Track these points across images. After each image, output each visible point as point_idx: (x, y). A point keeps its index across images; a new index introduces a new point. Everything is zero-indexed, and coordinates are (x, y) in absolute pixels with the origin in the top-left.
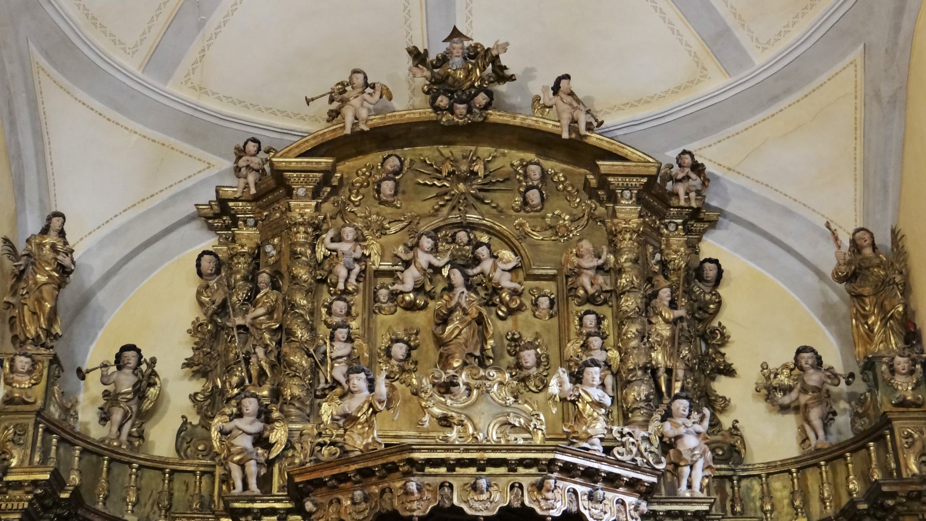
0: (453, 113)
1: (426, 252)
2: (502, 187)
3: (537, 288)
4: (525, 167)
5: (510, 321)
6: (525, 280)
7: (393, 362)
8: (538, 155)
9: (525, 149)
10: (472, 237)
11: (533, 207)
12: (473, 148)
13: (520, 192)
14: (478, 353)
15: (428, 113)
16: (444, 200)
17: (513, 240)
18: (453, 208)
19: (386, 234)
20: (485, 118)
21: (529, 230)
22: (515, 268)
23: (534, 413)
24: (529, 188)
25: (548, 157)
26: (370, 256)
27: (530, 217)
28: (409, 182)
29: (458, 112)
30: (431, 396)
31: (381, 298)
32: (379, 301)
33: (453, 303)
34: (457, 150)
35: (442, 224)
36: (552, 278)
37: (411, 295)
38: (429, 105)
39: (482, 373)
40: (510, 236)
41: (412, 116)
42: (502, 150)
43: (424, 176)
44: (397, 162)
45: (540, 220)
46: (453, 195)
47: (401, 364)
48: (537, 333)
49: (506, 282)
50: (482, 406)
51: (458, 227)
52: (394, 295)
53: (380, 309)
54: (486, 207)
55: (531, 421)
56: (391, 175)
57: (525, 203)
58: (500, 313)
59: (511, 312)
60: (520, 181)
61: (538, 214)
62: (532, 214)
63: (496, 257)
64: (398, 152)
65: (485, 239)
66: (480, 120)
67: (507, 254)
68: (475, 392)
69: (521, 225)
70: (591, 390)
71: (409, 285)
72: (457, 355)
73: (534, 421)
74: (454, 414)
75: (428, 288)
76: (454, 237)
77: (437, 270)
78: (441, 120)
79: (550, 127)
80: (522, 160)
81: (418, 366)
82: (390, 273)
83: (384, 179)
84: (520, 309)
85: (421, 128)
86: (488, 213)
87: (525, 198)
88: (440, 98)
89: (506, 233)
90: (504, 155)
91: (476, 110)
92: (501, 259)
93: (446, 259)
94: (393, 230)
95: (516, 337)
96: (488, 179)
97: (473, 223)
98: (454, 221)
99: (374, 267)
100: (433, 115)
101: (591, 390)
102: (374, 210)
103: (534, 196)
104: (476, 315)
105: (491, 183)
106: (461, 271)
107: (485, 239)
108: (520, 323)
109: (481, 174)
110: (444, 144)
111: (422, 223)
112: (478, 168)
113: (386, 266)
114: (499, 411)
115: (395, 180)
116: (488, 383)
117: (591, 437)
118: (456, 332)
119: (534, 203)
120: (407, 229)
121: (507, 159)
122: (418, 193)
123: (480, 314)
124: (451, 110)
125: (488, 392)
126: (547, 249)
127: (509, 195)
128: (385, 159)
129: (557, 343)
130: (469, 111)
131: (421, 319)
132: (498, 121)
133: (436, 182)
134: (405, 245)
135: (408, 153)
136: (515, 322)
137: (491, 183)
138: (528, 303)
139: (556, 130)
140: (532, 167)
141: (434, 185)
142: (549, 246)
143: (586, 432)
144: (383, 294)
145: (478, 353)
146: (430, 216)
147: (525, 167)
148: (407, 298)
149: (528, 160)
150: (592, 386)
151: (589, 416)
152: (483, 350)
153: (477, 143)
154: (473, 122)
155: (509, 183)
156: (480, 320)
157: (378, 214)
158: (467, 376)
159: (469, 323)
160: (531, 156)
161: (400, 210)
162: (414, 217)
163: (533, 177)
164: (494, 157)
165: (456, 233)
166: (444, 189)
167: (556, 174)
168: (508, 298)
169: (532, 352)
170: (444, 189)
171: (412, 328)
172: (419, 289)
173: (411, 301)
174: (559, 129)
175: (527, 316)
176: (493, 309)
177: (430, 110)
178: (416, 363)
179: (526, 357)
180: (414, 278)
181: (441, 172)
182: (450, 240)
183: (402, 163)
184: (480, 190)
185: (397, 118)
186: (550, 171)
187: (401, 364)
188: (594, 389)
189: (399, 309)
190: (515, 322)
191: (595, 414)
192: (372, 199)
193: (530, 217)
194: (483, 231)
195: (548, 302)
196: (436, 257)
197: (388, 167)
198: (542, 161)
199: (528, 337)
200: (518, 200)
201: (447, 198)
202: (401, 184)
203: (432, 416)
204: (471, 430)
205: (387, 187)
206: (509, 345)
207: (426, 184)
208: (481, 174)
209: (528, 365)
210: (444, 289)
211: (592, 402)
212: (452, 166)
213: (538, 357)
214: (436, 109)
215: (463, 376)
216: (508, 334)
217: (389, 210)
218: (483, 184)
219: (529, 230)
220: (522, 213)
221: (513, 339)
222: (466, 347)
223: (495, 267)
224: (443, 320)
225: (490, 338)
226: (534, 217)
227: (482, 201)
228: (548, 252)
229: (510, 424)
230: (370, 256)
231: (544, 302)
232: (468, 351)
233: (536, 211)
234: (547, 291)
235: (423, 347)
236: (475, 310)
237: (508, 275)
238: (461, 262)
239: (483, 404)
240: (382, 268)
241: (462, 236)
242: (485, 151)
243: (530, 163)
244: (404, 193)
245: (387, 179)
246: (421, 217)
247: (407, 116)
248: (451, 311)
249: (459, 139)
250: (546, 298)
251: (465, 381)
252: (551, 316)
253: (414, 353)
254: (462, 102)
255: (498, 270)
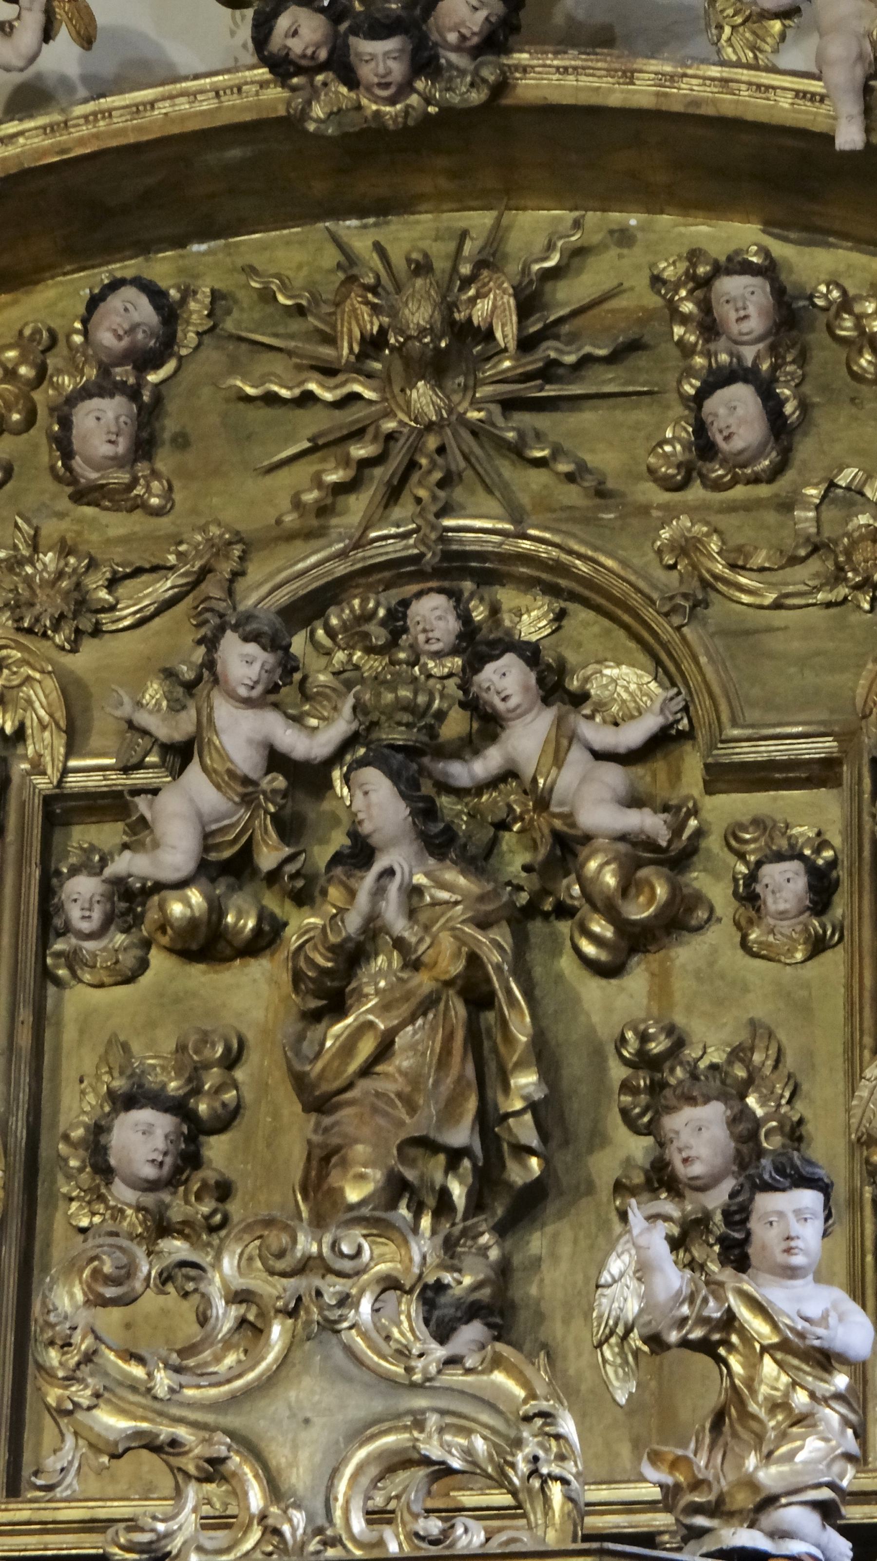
0: (351, 80)
1: (248, 703)
2: (608, 381)
3: (758, 823)
4: (702, 285)
5: (637, 981)
6: (710, 788)
7: (122, 1193)
8: (770, 225)
9: (712, 206)
10: (479, 614)
11: (738, 462)
12: (480, 221)
13: (684, 398)
14: (461, 1135)
15: (260, 93)
16: (346, 461)
17: (649, 614)
18: (394, 493)
19: (97, 631)
20: (501, 87)
21: (719, 568)
22: (662, 742)
23: (531, 1407)
24: (718, 379)
25: (816, 233)
26: (20, 734)
27: (732, 508)
28: (206, 391)
29: (366, 72)
30: (88, 1358)
31: (75, 913)
32: (67, 930)
33: (353, 923)
34: (410, 234)
35: (341, 569)
36: (821, 774)
37: (195, 896)
38: (250, 58)
39: (306, 1244)
40: (636, 600)
41: (183, 105)
42: (615, 217)
43: (278, 365)
44: (144, 311)
45: (771, 517)
46: (391, 437)
47: (149, 1199)
48: (753, 1025)
49: (597, 804)
50: (306, 1391)
51: (413, 577)
52: (129, 901)
53: (72, 959)
54: (538, 478)
55: (518, 1443)
56: (123, 373)
57: (704, 445)
58: (589, 949)
59: (638, 939)
60: (686, 350)
61: (763, 491)
62: (740, 492)
63: (580, 699)
64: (162, 267)
65: (532, 622)
66: (477, 97)
67: (625, 682)
68: (277, 1331)
69: (686, 548)
70: (779, 1295)
71: (175, 849)
72: (360, 1150)
73: (531, 1447)
74: (182, 1432)
75: (269, 855)
76: (397, 621)
77: (308, 778)
78: (304, 114)
79: (785, 102)
80: (694, 255)
81: (234, 1207)
82: (112, 805)
83: (85, 393)
84: (679, 919)
85: (235, 153)
86: (544, 504)
87: (701, 428)
88: (283, 22)
89: (619, 589)
90: (624, 238)
91: (453, 57)
92: (600, 707)
93: (341, 727)
94: (127, 614)
95: (656, 1047)
96: (549, 350)
97: (481, 556)
98: (393, 550)
99: (42, 783)
100: (275, 93)
101: (779, 1295)
102: (51, 529)
103: (738, 414)
104: (457, 968)
105: (549, 371)
106: (394, 776)
107: (532, 622)
108: (682, 986)
109: (506, 333)
110: (361, 212)
111: (255, 572)
112: (492, 308)
113: (93, 771)
114: (378, 1406)
115: (134, 394)
116: (332, 1288)
117: (770, 1501)
118: (366, 1047)
119: (738, 444)
120: (188, 601)
121: (637, 255)
122: (244, 438)
123: (474, 960)
124: (343, 67)
125: (330, 1327)
126: (796, 646)
127: (641, 415)
128: (94, 303)
129: (839, 1063)
130: (424, 61)
131: (251, 994)
132: (555, 98)
133: (312, 386)
134: (169, 674)
135: (199, 266)
136: (661, 989)
137: (549, 371)
138: (719, 894)
139: (810, 116)
140: (731, 285)
141: (307, 399)
142: (809, 631)
143: (751, 1484)
144: (82, 892)
145: (461, 1135)
146: (291, 537)
147: (702, 285)
148: (177, 909)
149: (719, 252)
150: (791, 1272)
151: (775, 1407)
152: (489, 1121)
153: (509, 193)
154: (447, 111)
155: (641, 360)
156: (476, 991)
157: (65, 549)
158: (245, 1263)
159: (428, 1004)
160: (744, 235)
161: (164, 523)
162: (220, 549)
163: (735, 329)
164: (579, 253)
165: (405, 604)
166: (354, 414)
167: (846, 304)
168: (610, 880)
169: (713, 1113)
170: (354, 414)
171: (205, 1039)
172: (225, 865)
173: (193, 923)
174: (824, 109)
175: (714, 950)
176: (564, 927)
177: (263, 73)
178: (223, 1191)
179: (686, 1137)
180: (201, 819)
181: (331, 340)
182: (379, 635)
183: (170, 314)
184: (510, 405)
185: (119, 121)
186: (826, 294)
187: (149, 1199)
188: (804, 1286)
189: (156, 957)
190: (661, 989)
191: (801, 1398)
192: (51, 485)
193: (732, 508)
194: (528, 584)
195: (800, 883)
196: (297, 720)
197: (106, 338)
198: (780, 249)
199: (710, 1047)
200: (675, 436)
201: (360, 451)
202: (172, 406)
203: (95, 1448)
204: (256, 1499)
205: (101, 425)
206: (626, 1087)
207: (271, 399)
208: (506, 333)
209: (697, 1169)
210: (337, 859)
211: (784, 1346)
212: (376, 309)
213: (745, 1132)
214: (282, 67)
215: (228, 1264)
216: (622, 1040)
217: (117, 524)
218: (526, 377)
219: (719, 568)
220: (696, 492)
221: (644, 1061)
222: (412, 1108)
223: (561, 743)
224: (328, 993)
225: (520, 1065)
226: (747, 506)
227: (517, 452)
228: (803, 662)
229: (426, 1461)
230: (20, 734)
231: (785, 884)
232: (414, 1126)
233: (756, 480)
234: (803, 831)
235: (257, 1118)
236: (447, 941)
237: (613, 776)
238: (399, 736)
239: (307, 1381)
240: (75, 782)
241: (433, 615)
242: (537, 228)
243: (737, 265)
244: (182, 442)
245: (104, 387)
246: (248, 546)
247: (164, 108)
248: (353, 956)
249: (425, 185)
250: (794, 867)
251: (239, 1283)
252: (818, 946)
253: (216, 1149)
254: (379, 30)
255: (577, 756)
